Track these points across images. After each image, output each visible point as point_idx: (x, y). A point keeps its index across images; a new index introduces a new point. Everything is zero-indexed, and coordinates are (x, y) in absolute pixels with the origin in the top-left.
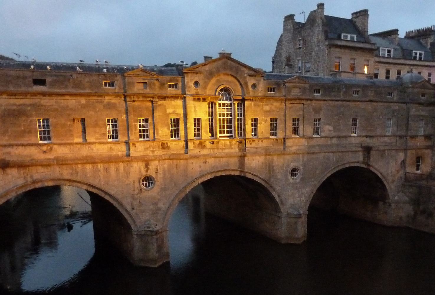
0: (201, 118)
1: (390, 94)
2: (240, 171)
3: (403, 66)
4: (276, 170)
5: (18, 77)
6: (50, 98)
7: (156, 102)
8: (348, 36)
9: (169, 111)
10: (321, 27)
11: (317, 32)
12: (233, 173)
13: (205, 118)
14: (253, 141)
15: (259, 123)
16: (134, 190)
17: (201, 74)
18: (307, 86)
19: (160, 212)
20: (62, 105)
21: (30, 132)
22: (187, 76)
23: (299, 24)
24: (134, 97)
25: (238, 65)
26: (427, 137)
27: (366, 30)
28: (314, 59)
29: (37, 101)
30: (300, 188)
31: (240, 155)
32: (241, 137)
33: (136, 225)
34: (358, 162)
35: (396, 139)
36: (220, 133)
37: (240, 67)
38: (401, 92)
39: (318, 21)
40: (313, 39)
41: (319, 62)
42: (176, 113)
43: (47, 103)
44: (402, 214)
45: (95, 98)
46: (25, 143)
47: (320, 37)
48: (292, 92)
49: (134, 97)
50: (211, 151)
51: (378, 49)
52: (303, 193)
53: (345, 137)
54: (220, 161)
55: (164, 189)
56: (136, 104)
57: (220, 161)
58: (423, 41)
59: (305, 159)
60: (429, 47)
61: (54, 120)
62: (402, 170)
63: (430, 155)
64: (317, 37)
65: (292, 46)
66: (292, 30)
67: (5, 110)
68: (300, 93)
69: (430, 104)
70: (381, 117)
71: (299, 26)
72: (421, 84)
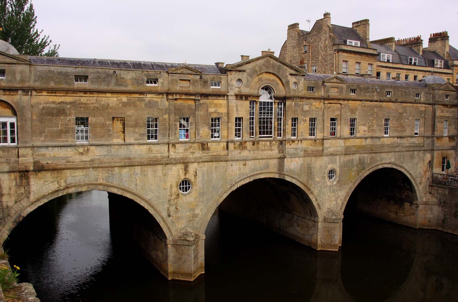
0: (242, 118)
1: (417, 95)
2: (279, 173)
3: (401, 71)
4: (315, 172)
5: (60, 73)
6: (91, 95)
7: (200, 100)
8: (353, 43)
9: (211, 110)
10: (328, 34)
11: (323, 39)
12: (272, 176)
13: (246, 116)
14: (293, 141)
15: (298, 123)
16: (171, 196)
17: (244, 73)
18: (344, 86)
19: (197, 219)
20: (102, 103)
21: (67, 132)
22: (231, 75)
23: (302, 31)
24: (176, 95)
25: (279, 64)
26: (451, 138)
27: (367, 37)
28: (321, 63)
29: (77, 98)
30: (337, 191)
31: (279, 157)
32: (253, 137)
33: (171, 234)
34: (390, 163)
35: (424, 140)
36: (260, 134)
37: (282, 65)
38: (427, 93)
39: (325, 28)
40: (320, 44)
41: (326, 65)
42: (218, 112)
43: (87, 100)
44: (430, 215)
45: (137, 96)
46: (62, 144)
47: (327, 42)
48: (330, 92)
49: (176, 95)
50: (252, 152)
51: (379, 55)
52: (339, 197)
53: (379, 138)
54: (150, 150)
55: (202, 194)
56: (179, 102)
57: (150, 150)
58: (415, 49)
59: (342, 160)
60: (421, 54)
61: (439, 65)
62: (429, 171)
63: (453, 156)
64: (323, 43)
65: (297, 51)
66: (297, 37)
67: (43, 108)
68: (338, 93)
69: (453, 106)
70: (410, 118)
71: (304, 35)
72: (445, 86)
